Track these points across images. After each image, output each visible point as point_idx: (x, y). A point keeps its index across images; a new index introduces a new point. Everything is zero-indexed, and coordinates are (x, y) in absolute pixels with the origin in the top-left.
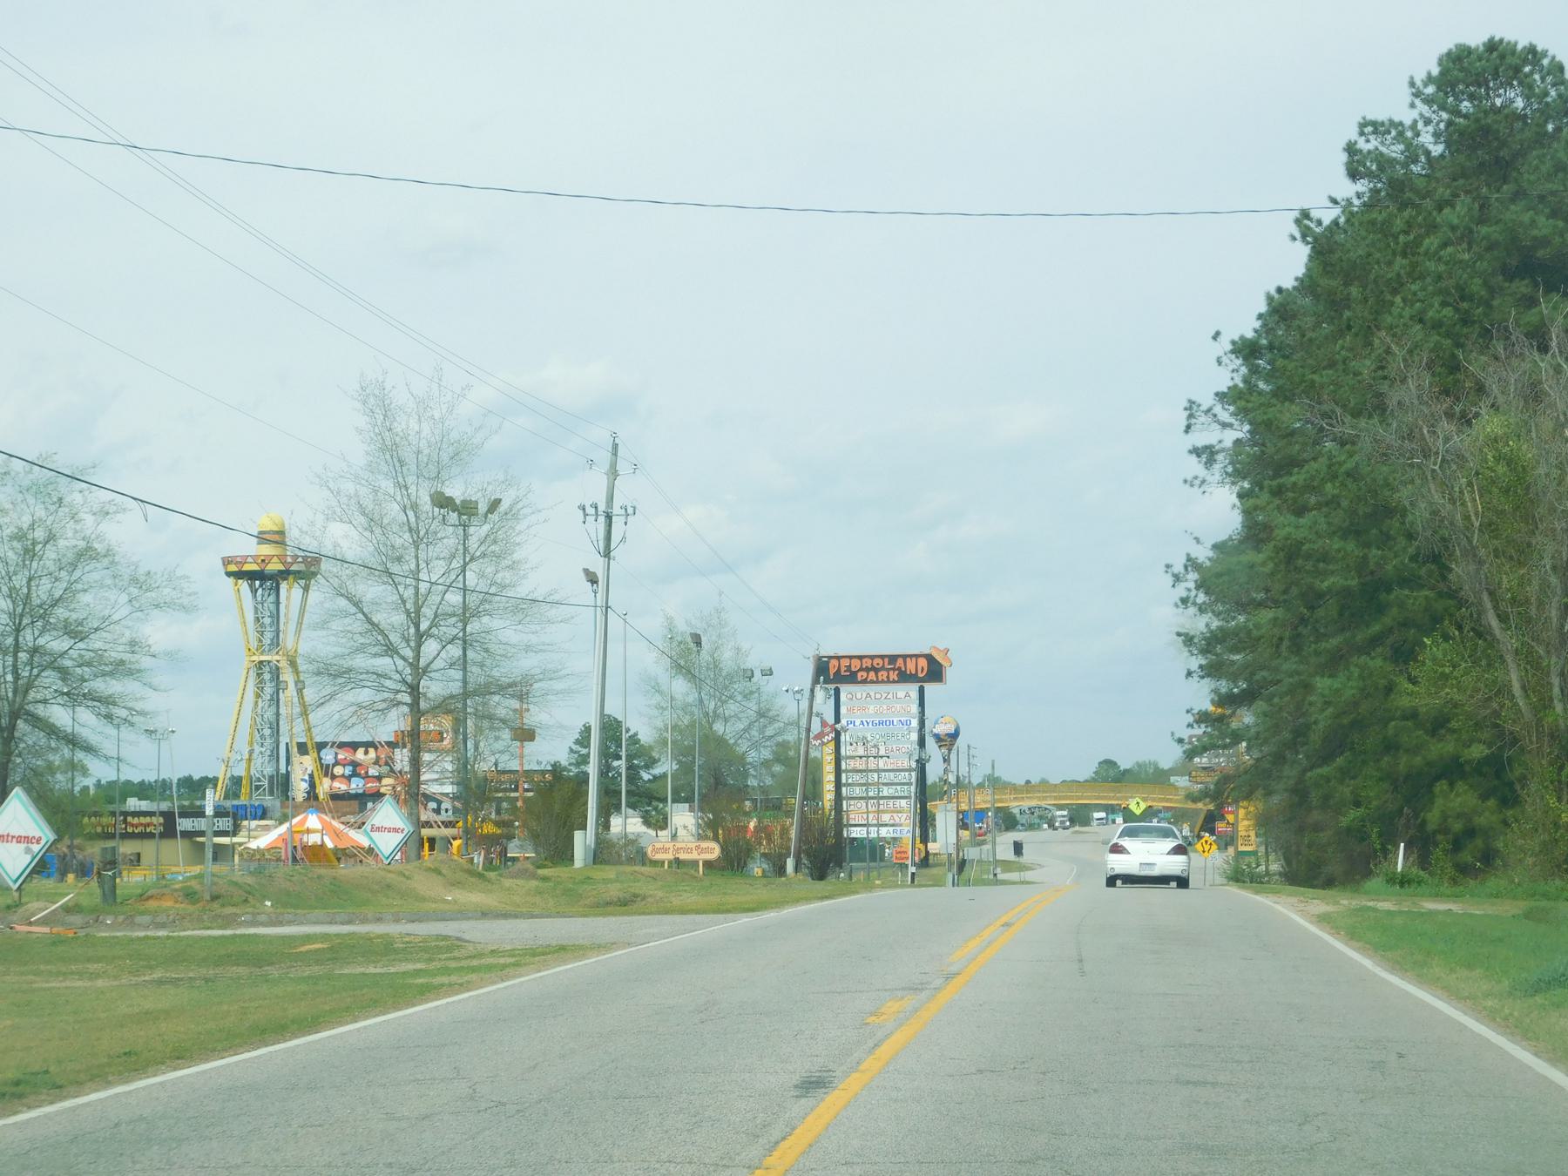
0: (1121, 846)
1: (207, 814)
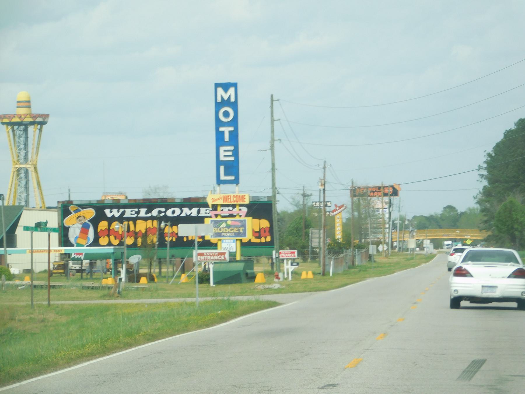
0: (465, 270)
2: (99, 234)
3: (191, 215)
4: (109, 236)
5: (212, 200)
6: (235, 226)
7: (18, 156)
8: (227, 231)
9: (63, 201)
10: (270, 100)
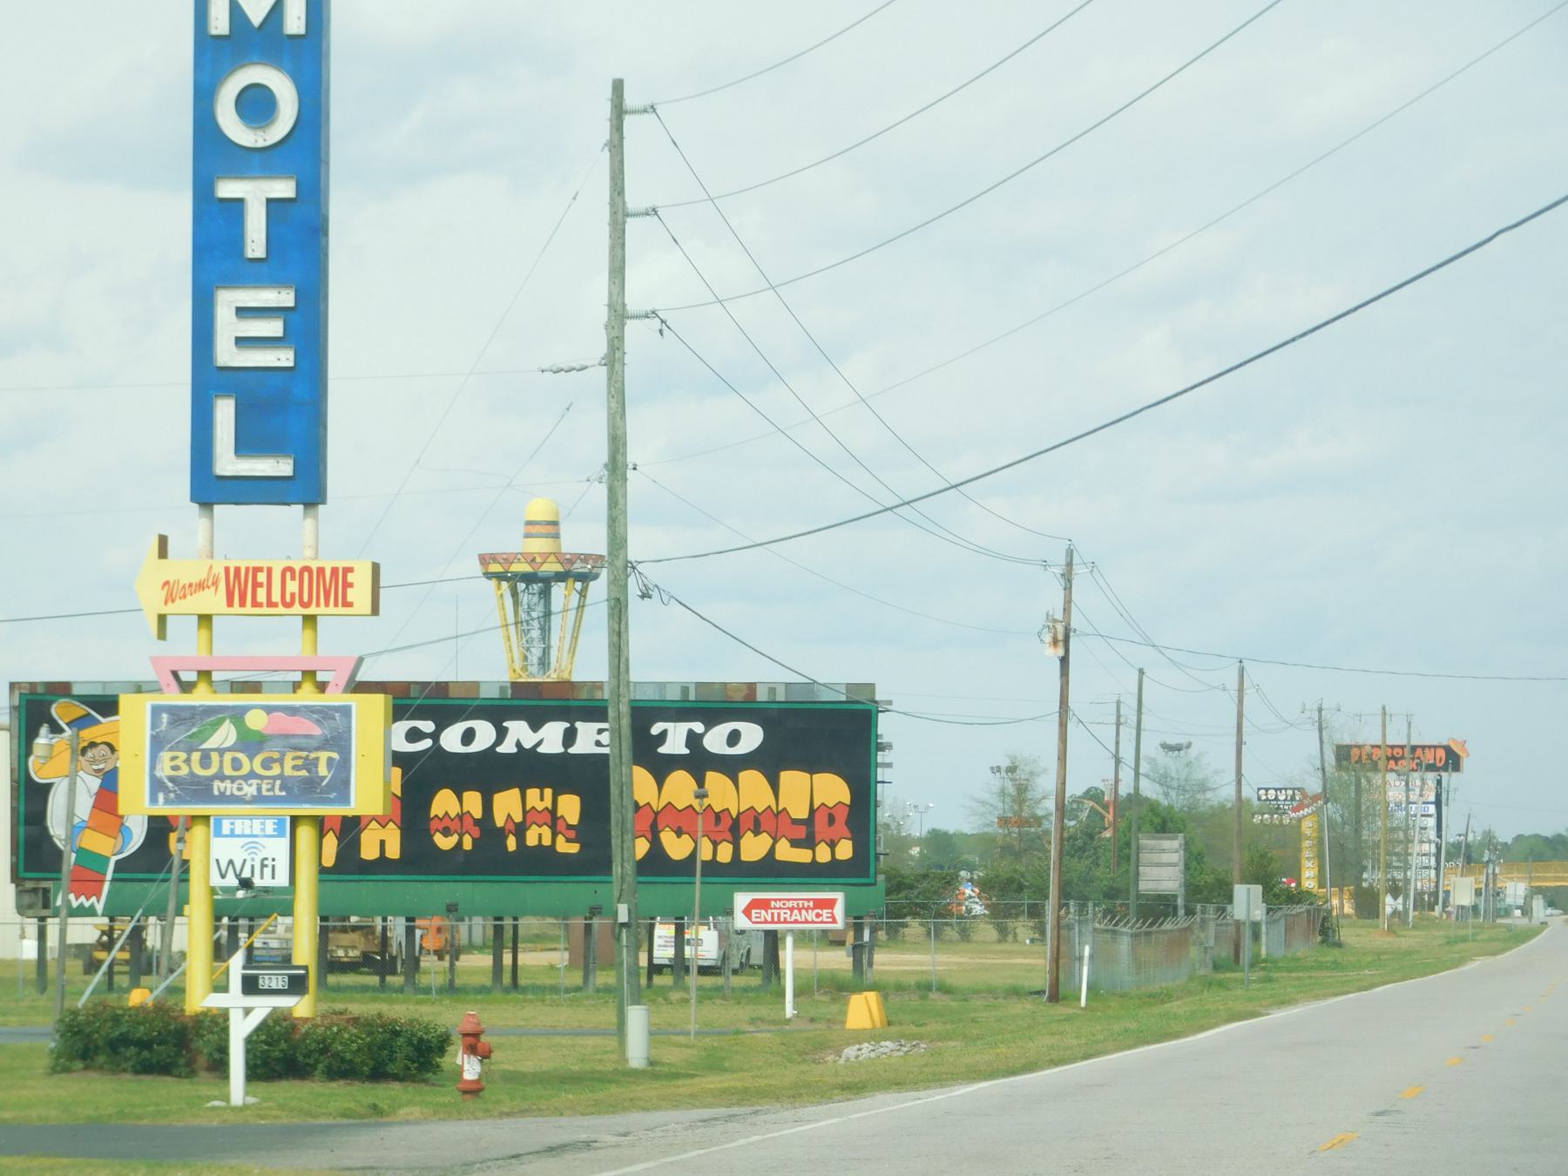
1: (177, 918)
5: (164, 593)
6: (293, 743)
7: (526, 658)
8: (245, 770)
9: (31, 683)
10: (606, 109)
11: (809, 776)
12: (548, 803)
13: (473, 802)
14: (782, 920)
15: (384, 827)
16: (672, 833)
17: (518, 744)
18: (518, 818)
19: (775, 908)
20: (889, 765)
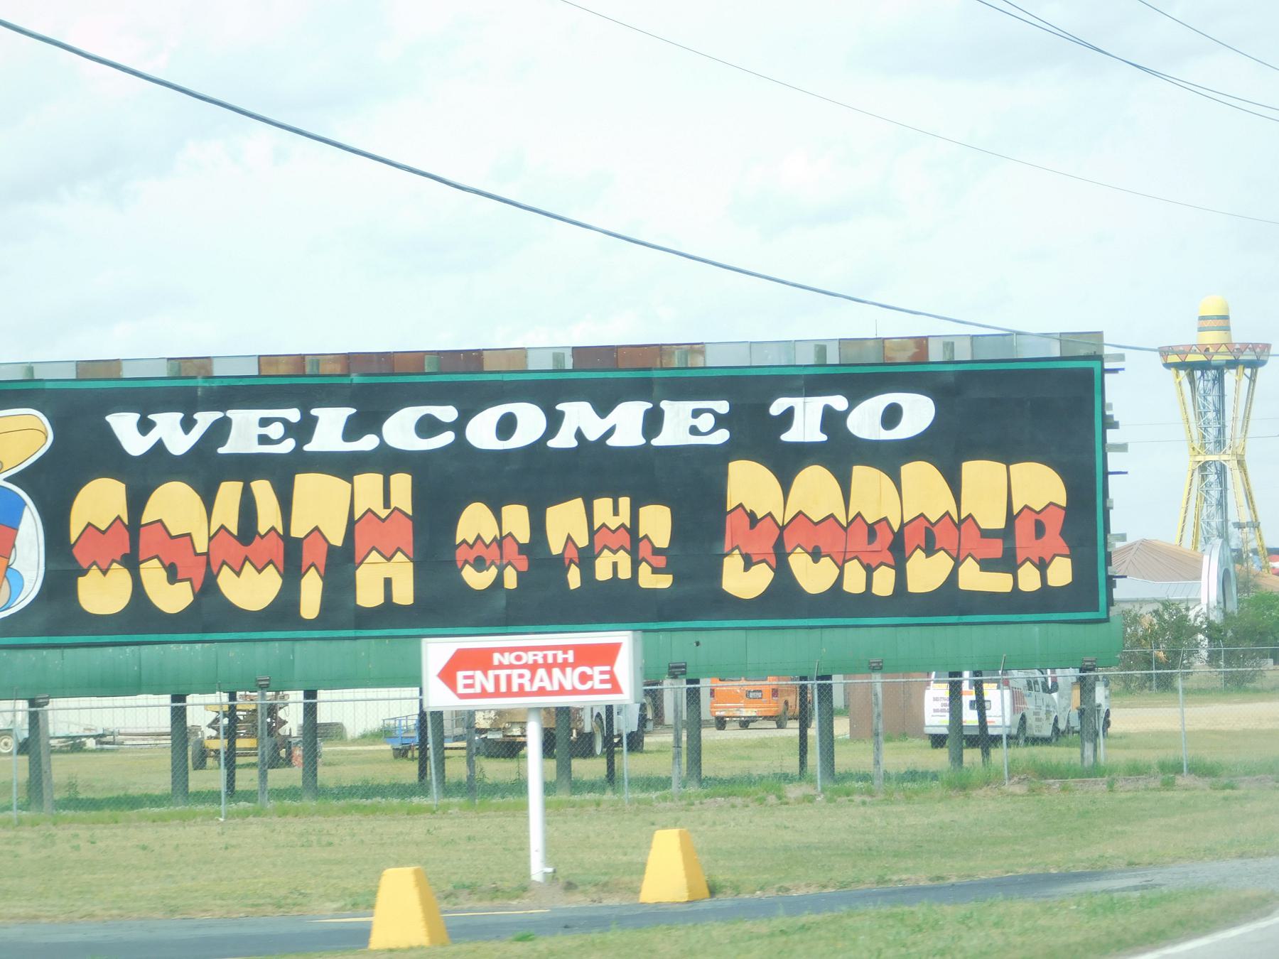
2: (75, 551)
3: (610, 442)
4: (132, 563)
7: (1204, 437)
11: (1002, 467)
12: (625, 517)
13: (517, 519)
14: (515, 688)
15: (389, 559)
16: (806, 554)
17: (579, 435)
18: (582, 541)
19: (501, 666)
20: (1122, 448)
